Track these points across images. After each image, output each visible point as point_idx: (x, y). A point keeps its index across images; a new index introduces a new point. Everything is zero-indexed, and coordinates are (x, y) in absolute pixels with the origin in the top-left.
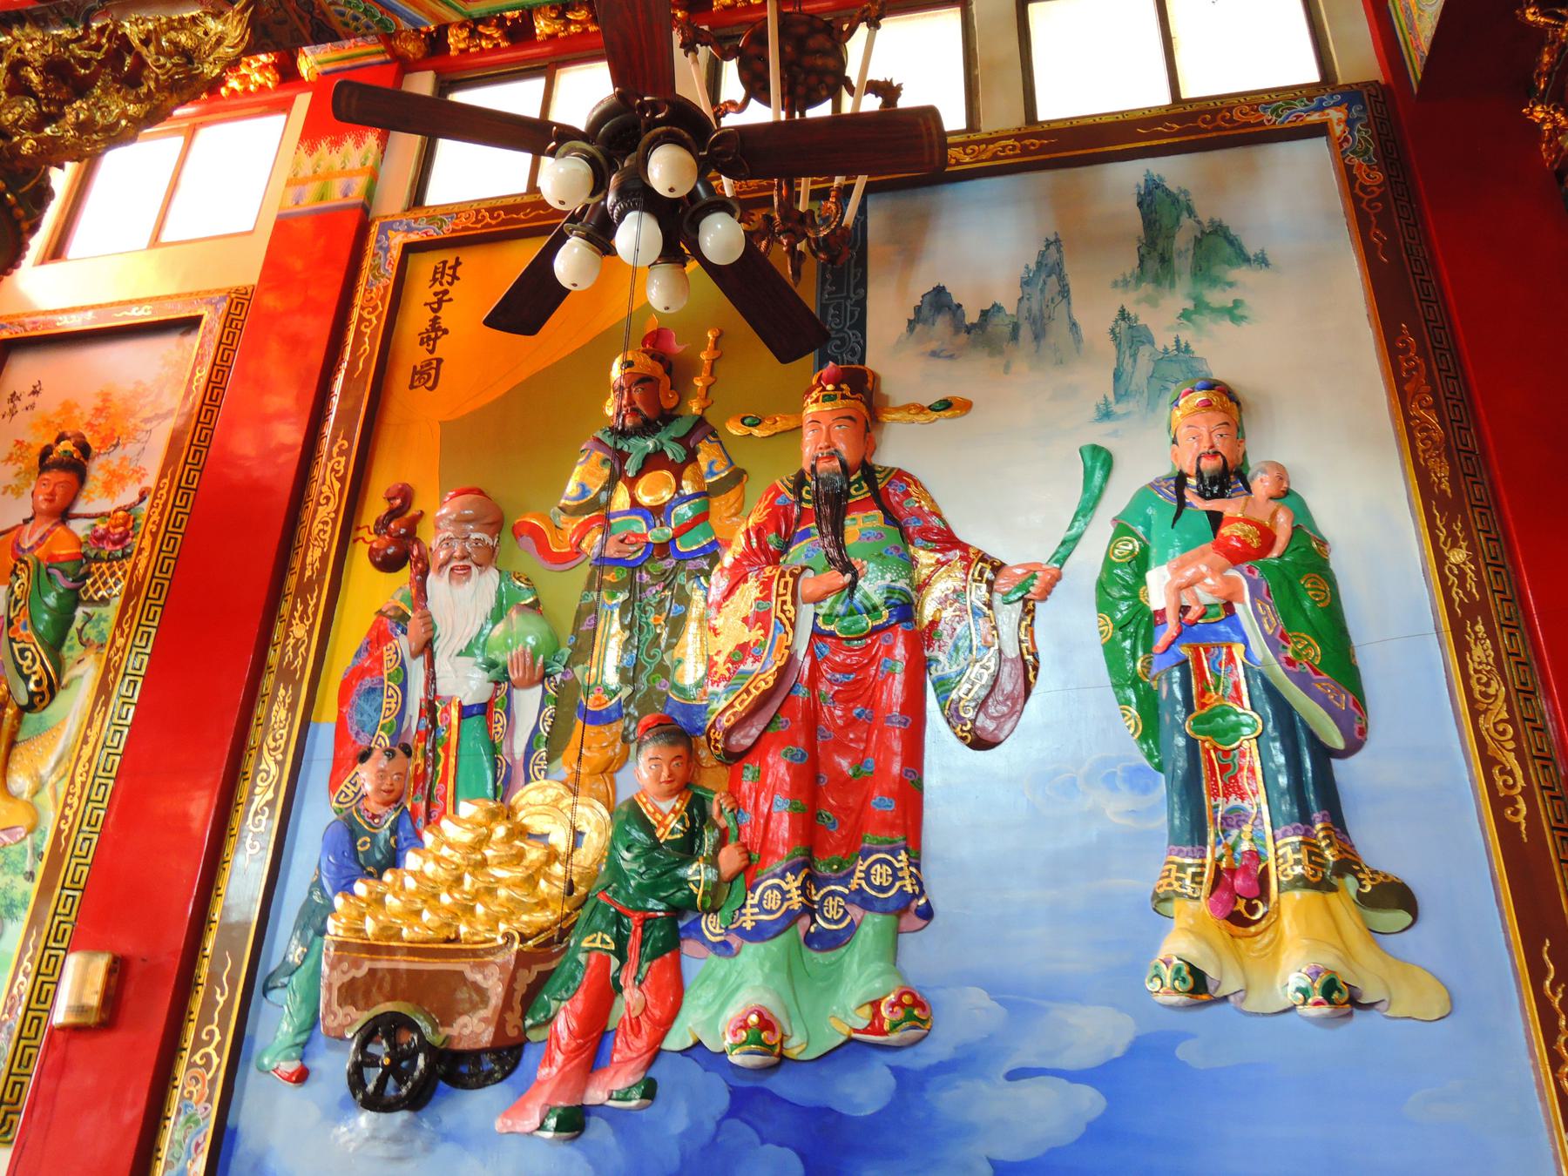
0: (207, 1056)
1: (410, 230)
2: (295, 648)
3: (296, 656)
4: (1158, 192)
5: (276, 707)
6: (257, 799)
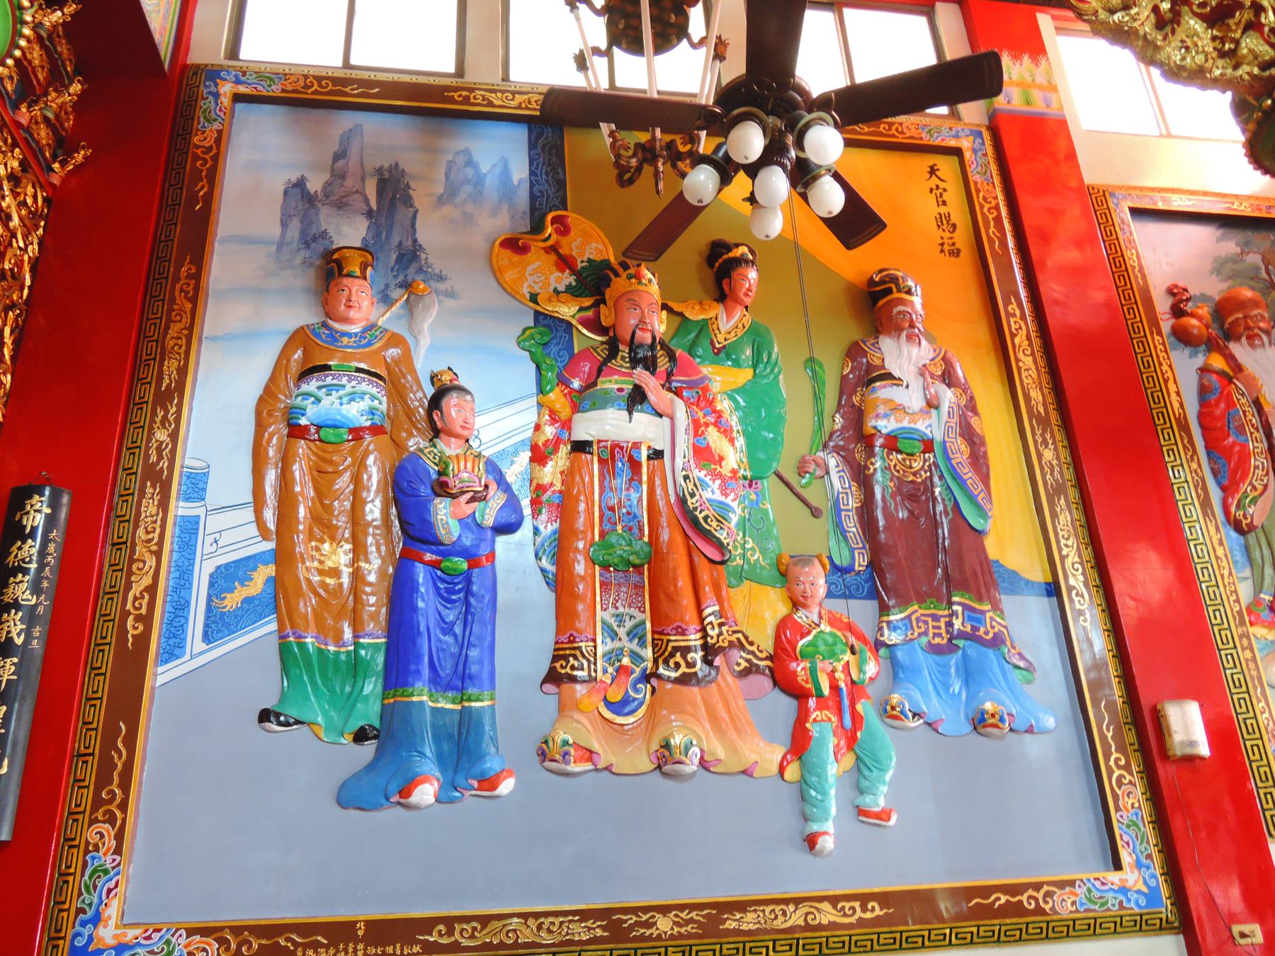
0: (112, 792)
1: (974, 151)
2: (159, 450)
3: (160, 458)
4: (1225, 482)
5: (744, 927)
6: (832, 919)
